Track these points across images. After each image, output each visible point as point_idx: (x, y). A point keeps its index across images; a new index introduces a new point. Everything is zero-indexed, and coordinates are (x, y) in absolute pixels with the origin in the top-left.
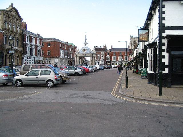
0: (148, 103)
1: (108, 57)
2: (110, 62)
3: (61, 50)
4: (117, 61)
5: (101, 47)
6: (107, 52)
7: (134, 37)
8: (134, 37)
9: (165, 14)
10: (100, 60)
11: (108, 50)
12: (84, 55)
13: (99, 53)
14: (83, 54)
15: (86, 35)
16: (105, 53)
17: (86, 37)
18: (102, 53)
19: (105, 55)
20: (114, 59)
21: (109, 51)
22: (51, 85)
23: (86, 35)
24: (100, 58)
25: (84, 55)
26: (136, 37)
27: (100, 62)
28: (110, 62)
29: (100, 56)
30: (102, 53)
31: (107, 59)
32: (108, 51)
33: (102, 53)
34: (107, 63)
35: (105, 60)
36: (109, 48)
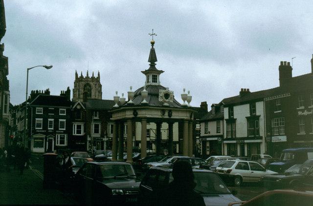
2: (84, 138)
3: (272, 141)
4: (102, 136)
7: (85, 76)
9: (206, 102)
10: (54, 133)
12: (167, 114)
13: (51, 111)
14: (163, 112)
15: (153, 43)
18: (63, 112)
20: (96, 131)
23: (153, 43)
24: (56, 128)
25: (167, 114)
28: (84, 138)
29: (56, 121)
31: (75, 129)
32: (78, 107)
33: (63, 111)
34: (72, 139)
35: (69, 131)
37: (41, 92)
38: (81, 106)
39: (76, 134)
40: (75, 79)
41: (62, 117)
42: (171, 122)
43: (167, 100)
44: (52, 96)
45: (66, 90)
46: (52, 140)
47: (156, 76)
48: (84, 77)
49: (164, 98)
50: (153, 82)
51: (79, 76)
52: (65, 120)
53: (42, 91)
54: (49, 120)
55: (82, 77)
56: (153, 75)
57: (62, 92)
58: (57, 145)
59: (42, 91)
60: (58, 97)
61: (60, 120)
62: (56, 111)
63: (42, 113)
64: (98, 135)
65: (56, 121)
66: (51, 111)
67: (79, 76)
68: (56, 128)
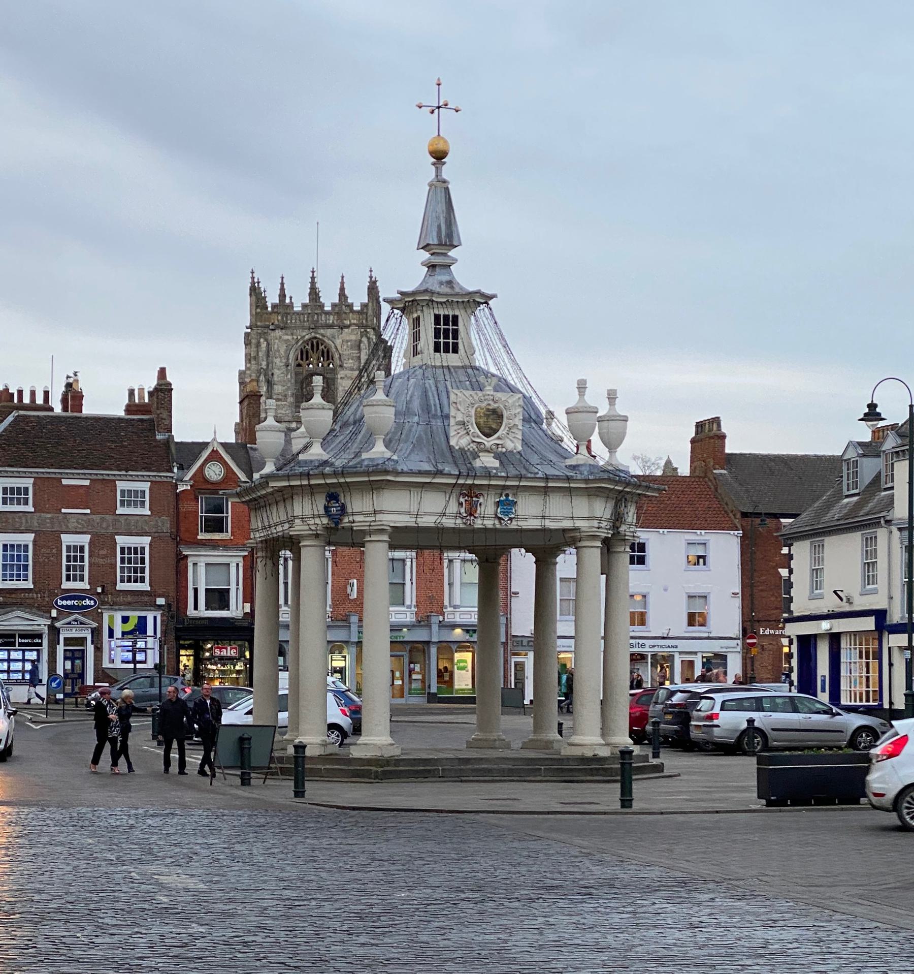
0: (471, 778)
1: (217, 557)
5: (72, 396)
6: (201, 483)
7: (299, 298)
8: (299, 298)
11: (214, 456)
13: (76, 497)
14: (471, 494)
15: (439, 156)
16: (165, 495)
17: (441, 192)
18: (133, 498)
19: (180, 530)
21: (230, 476)
22: (338, 736)
23: (439, 156)
26: (329, 299)
27: (96, 633)
29: (103, 543)
30: (133, 498)
32: (214, 472)
33: (134, 488)
36: (878, 410)
37: (26, 400)
38: (225, 464)
39: (203, 612)
40: (246, 320)
41: (133, 527)
42: (490, 555)
43: (489, 442)
44: (87, 418)
45: (151, 383)
46: (82, 641)
47: (455, 319)
48: (297, 308)
49: (474, 429)
50: (437, 349)
51: (272, 299)
52: (145, 541)
53: (33, 394)
54: (67, 539)
55: (283, 306)
56: (437, 317)
57: (131, 393)
58: (106, 664)
59: (33, 394)
60: (120, 420)
61: (122, 541)
62: (100, 497)
63: (30, 508)
64: (405, 614)
65: (103, 543)
66: (76, 497)
67: (272, 299)
68: (103, 579)
